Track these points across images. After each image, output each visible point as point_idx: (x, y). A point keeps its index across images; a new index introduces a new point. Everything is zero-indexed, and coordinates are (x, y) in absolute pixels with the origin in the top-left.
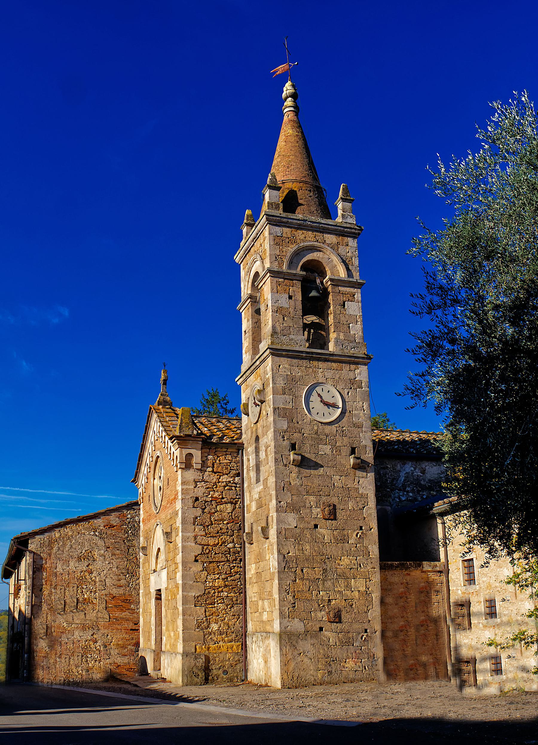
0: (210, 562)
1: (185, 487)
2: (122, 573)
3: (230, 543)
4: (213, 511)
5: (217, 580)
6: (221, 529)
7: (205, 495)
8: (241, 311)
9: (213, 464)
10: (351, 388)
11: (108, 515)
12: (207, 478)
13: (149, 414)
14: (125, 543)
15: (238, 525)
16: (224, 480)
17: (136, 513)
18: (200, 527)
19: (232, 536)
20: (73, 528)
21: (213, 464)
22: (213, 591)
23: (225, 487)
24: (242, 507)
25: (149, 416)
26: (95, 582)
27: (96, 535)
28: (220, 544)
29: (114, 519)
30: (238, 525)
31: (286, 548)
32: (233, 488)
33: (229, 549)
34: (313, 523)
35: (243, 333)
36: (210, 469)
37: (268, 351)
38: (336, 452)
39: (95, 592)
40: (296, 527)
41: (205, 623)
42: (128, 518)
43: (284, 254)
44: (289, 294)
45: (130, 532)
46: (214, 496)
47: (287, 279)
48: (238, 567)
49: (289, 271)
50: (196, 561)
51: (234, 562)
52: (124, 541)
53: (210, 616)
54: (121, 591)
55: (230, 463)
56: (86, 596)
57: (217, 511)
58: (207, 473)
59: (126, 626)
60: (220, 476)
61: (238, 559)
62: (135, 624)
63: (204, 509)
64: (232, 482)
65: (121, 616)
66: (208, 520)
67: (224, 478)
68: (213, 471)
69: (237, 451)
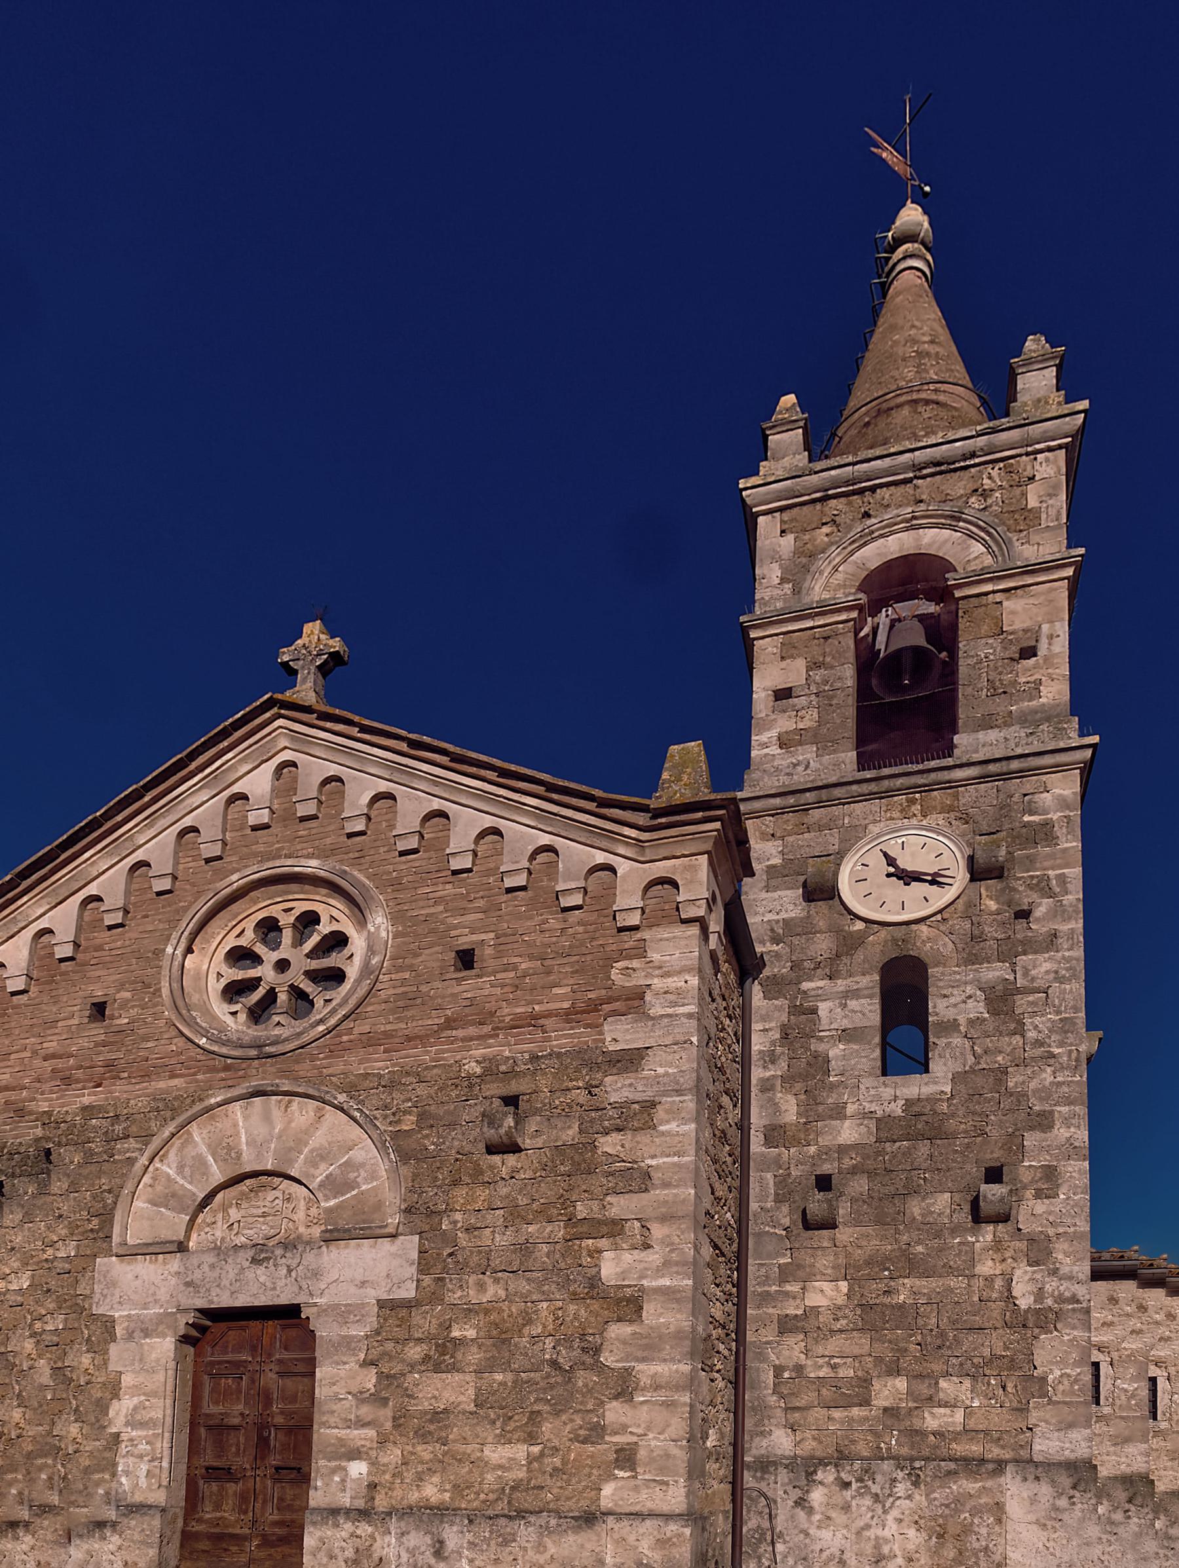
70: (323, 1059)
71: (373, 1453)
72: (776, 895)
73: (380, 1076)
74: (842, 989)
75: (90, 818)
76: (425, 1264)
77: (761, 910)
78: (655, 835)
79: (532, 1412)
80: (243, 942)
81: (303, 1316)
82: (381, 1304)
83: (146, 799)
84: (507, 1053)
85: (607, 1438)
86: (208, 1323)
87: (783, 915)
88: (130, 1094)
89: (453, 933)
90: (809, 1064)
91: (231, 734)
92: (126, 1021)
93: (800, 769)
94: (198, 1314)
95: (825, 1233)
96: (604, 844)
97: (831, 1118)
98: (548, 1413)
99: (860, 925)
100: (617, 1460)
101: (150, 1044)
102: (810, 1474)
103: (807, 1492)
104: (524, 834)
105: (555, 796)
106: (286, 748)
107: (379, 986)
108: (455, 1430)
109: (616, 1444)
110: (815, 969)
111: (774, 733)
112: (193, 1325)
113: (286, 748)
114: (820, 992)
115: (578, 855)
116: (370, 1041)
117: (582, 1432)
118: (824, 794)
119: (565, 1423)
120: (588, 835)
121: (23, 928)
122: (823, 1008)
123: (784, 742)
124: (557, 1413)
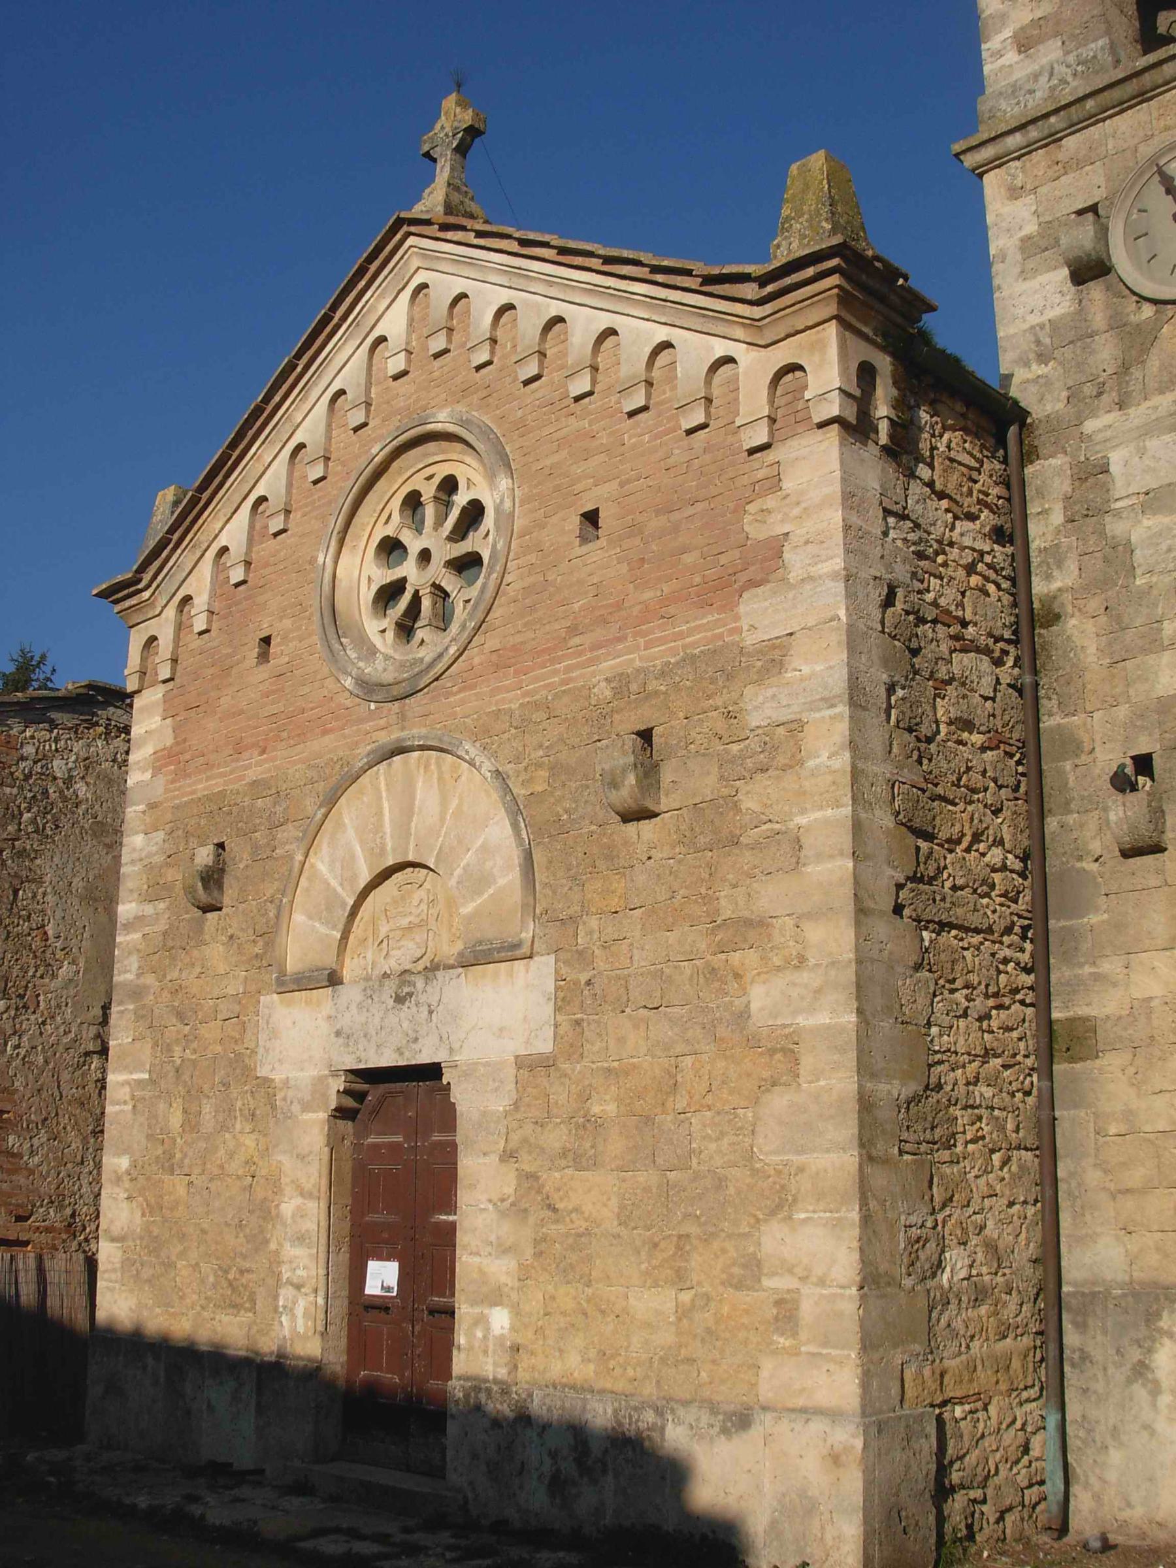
13: (371, 259)
16: (967, 541)
17: (57, 740)
25: (361, 272)
28: (964, 844)
37: (836, 291)
42: (23, 758)
45: (27, 816)
58: (916, 489)
62: (20, 1219)
70: (460, 691)
71: (514, 1296)
72: (1034, 283)
73: (511, 713)
74: (1137, 422)
75: (252, 406)
76: (565, 997)
77: (1020, 311)
78: (768, 308)
79: (680, 1237)
80: (390, 531)
81: (445, 1082)
82: (521, 1063)
83: (299, 369)
84: (638, 664)
85: (766, 1282)
86: (366, 1087)
87: (1051, 314)
88: (290, 762)
89: (578, 487)
90: (1106, 560)
91: (368, 269)
92: (287, 659)
93: (1043, 80)
94: (351, 1077)
95: (1148, 859)
96: (721, 329)
97: (1145, 651)
98: (699, 1238)
99: (1148, 311)
100: (776, 1319)
101: (306, 690)
102: (1151, 1318)
103: (1150, 1351)
104: (640, 332)
105: (660, 278)
106: (419, 268)
107: (508, 578)
108: (598, 1262)
109: (776, 1290)
110: (1100, 394)
111: (1007, 33)
112: (347, 1092)
113: (419, 268)
114: (1109, 433)
115: (696, 349)
116: (501, 662)
117: (736, 1270)
118: (1075, 113)
119: (717, 1256)
120: (702, 320)
121: (206, 550)
122: (1116, 459)
123: (1024, 44)
124: (707, 1239)
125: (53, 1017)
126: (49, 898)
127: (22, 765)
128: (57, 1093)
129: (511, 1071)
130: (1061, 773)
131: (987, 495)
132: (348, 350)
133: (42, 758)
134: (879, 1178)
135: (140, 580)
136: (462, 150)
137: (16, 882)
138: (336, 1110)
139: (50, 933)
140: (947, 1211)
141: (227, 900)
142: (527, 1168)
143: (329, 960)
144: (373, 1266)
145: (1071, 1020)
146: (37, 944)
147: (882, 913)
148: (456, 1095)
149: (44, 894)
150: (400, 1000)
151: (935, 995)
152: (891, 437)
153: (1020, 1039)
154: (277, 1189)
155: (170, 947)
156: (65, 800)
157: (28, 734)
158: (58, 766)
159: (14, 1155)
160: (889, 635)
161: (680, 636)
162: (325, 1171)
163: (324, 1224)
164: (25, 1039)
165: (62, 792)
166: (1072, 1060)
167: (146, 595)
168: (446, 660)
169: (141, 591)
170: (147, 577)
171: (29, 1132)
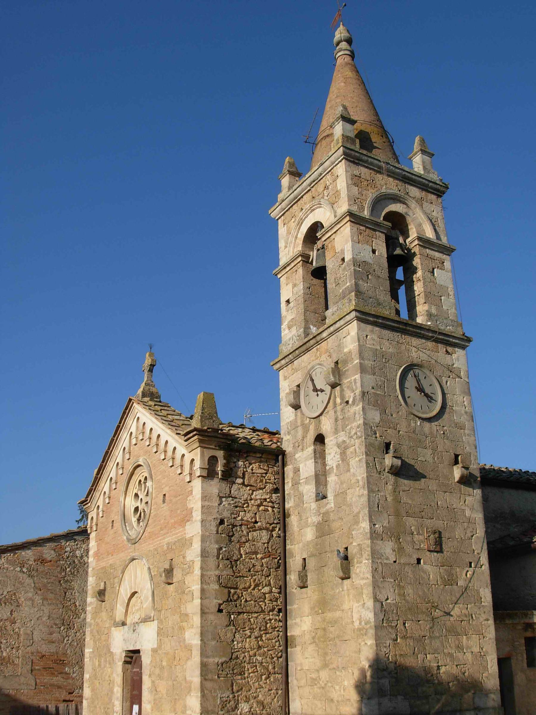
0: (239, 613)
1: (206, 503)
2: (56, 624)
3: (266, 585)
4: (244, 539)
5: (248, 640)
6: (254, 566)
7: (233, 516)
8: (279, 276)
9: (244, 474)
10: (449, 377)
11: (41, 546)
12: (236, 493)
14: (61, 584)
15: (276, 560)
16: (258, 497)
17: (77, 545)
18: (226, 562)
19: (268, 576)
20: (9, 558)
21: (244, 474)
22: (243, 655)
23: (259, 506)
24: (282, 535)
26: (18, 635)
27: (24, 572)
28: (252, 587)
29: (48, 551)
30: (276, 560)
31: (384, 592)
32: (270, 509)
33: (264, 594)
34: (415, 557)
35: (283, 305)
36: (239, 481)
37: (353, 314)
38: (438, 458)
39: (18, 648)
40: (395, 562)
41: (232, 703)
42: (66, 552)
43: (364, 197)
44: (372, 246)
46: (245, 519)
47: (370, 228)
48: (276, 620)
49: (372, 218)
50: (220, 611)
51: (271, 613)
52: (60, 581)
53: (238, 691)
54: (53, 648)
55: (266, 473)
56: (4, 654)
57: (249, 540)
58: (235, 487)
59: (57, 695)
60: (253, 491)
61: (276, 610)
62: (70, 693)
63: (232, 536)
64: (268, 500)
65: (52, 682)
66: (237, 552)
67: (258, 495)
68: (243, 484)
69: (274, 458)
89: (163, 487)
107: (152, 512)
125: (79, 631)
126: (76, 594)
127: (66, 554)
128: (81, 654)
129: (150, 653)
130: (289, 562)
131: (270, 480)
132: (125, 435)
133: (73, 551)
134: (209, 685)
135: (87, 500)
136: (151, 371)
137: (65, 590)
138: (124, 661)
139: (77, 605)
140: (240, 693)
141: (106, 599)
142: (153, 679)
143: (123, 618)
144: (134, 706)
145: (291, 636)
146: (73, 608)
147: (212, 613)
148: (143, 659)
149: (75, 593)
150: (134, 631)
151: (235, 633)
152: (222, 475)
153: (276, 642)
154: (114, 685)
155: (96, 612)
156: (81, 563)
157: (67, 544)
158: (78, 553)
159: (67, 674)
160: (236, 526)
161: (177, 534)
162: (122, 679)
163: (122, 695)
164: (70, 638)
165: (79, 561)
166: (292, 648)
167: (89, 504)
168: (141, 534)
169: (88, 503)
170: (89, 499)
171: (73, 666)
